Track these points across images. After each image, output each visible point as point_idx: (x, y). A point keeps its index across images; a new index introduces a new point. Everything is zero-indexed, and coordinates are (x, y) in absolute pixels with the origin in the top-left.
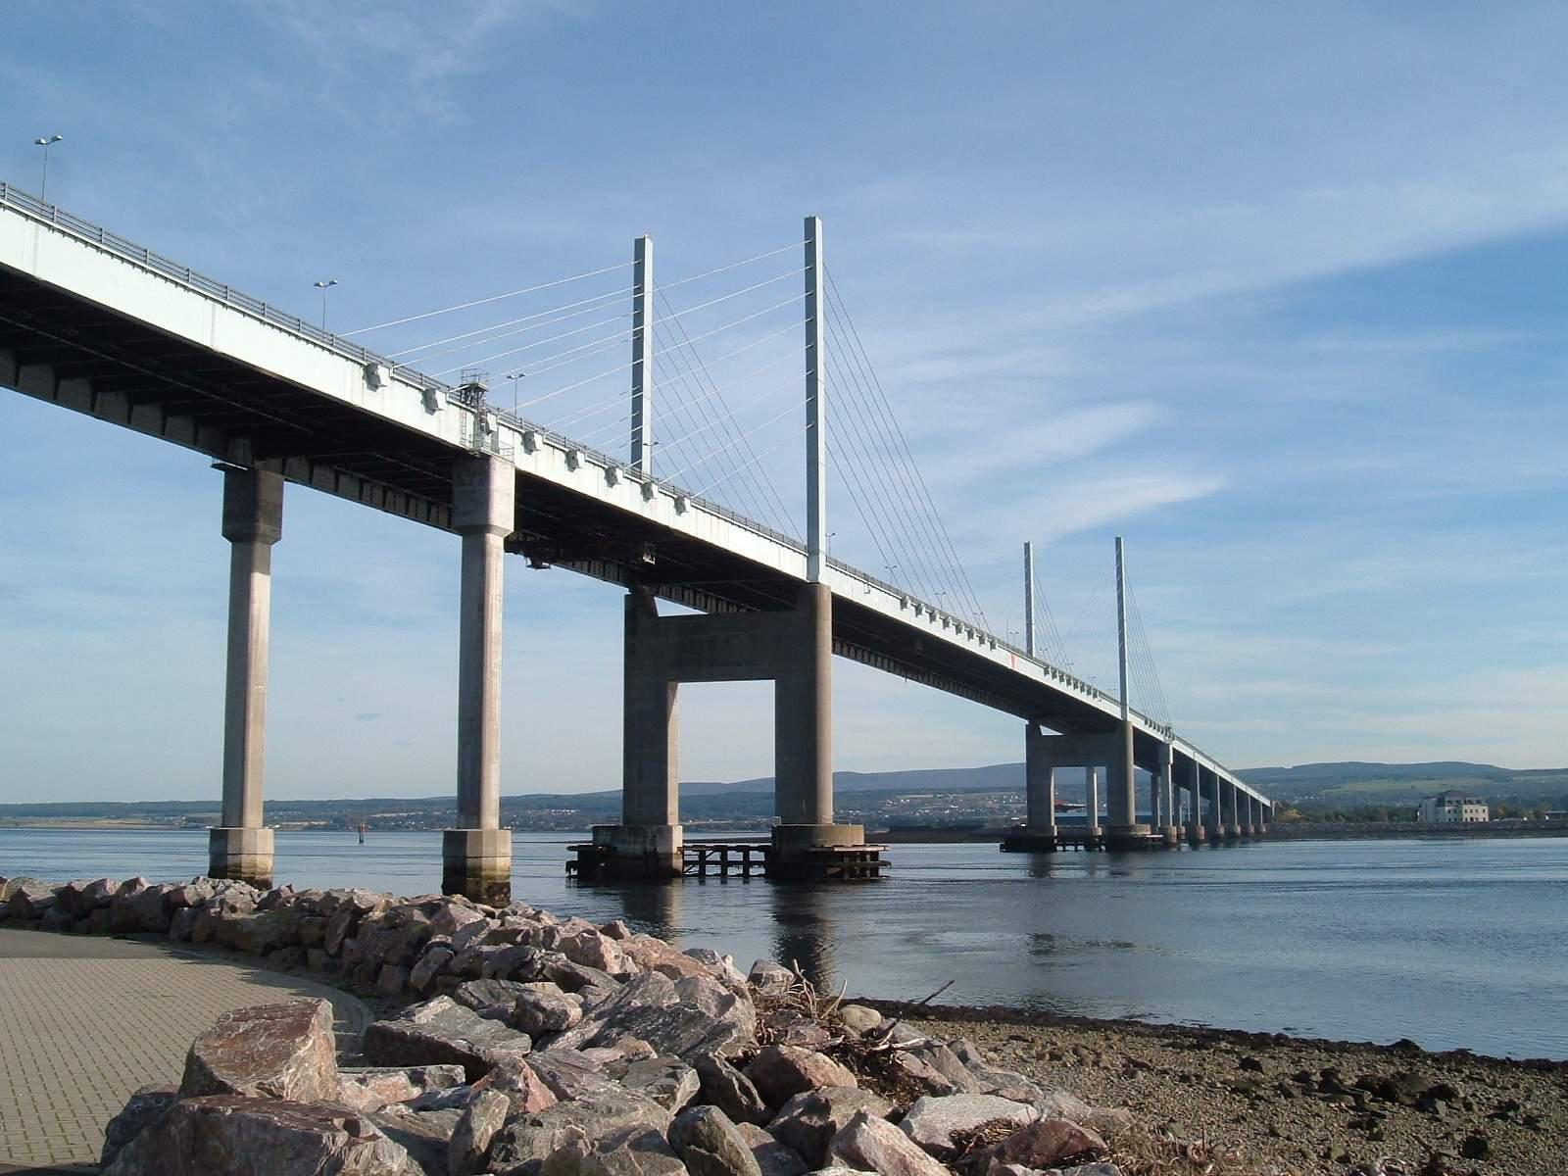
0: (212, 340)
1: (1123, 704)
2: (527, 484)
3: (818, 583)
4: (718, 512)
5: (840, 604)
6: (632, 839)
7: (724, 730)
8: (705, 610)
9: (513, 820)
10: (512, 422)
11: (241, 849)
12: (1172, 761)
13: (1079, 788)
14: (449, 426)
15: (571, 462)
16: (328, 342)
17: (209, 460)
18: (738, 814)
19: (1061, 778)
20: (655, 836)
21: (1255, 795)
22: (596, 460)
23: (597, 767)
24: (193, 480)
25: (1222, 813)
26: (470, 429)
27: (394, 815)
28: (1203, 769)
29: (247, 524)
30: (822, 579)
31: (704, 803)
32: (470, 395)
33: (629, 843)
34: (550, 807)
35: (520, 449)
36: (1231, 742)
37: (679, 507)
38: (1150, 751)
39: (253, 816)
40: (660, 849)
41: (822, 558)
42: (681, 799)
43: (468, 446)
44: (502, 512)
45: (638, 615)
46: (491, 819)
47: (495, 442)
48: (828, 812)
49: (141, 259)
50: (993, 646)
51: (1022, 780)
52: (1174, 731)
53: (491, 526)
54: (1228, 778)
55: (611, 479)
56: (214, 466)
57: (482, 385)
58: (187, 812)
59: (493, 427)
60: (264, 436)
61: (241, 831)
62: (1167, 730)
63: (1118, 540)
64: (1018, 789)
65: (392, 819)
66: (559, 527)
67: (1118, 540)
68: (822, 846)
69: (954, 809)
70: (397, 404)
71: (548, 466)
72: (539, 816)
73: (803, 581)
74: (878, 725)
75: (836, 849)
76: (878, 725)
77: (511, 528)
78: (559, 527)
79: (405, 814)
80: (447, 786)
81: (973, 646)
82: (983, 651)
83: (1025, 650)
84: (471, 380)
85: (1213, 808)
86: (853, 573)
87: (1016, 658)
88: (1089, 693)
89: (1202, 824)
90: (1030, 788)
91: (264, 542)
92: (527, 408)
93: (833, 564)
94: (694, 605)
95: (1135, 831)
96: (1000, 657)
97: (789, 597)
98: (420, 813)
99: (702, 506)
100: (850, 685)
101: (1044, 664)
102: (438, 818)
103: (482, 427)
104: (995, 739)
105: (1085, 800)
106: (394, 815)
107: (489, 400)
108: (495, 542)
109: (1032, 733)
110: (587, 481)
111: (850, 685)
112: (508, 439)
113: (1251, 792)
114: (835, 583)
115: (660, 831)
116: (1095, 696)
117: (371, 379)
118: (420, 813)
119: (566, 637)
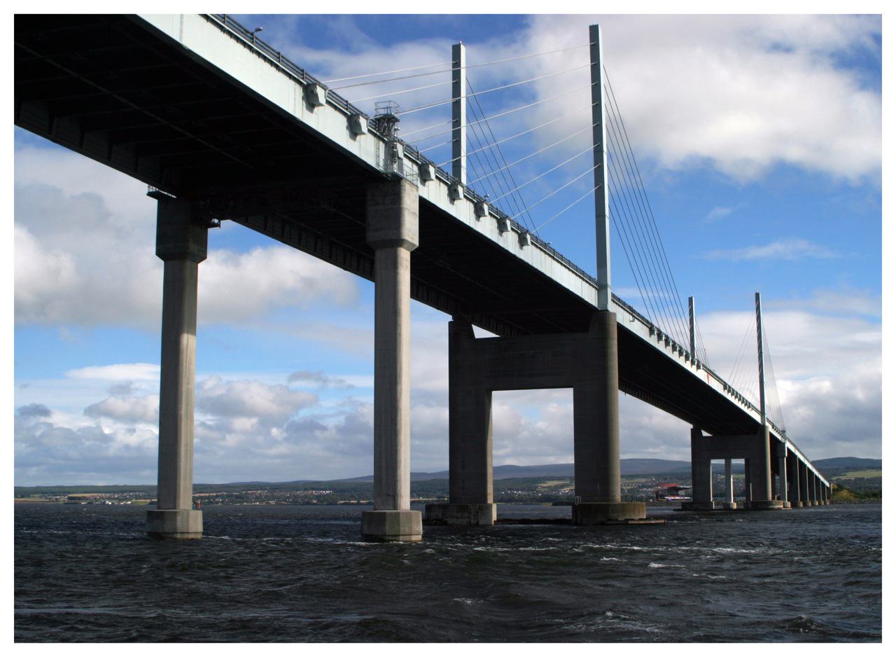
0: (181, 37)
1: (601, 287)
2: (426, 208)
3: (607, 310)
6: (460, 515)
7: (533, 425)
9: (288, 498)
11: (176, 529)
12: (786, 455)
13: (729, 472)
14: (367, 150)
18: (440, 494)
20: (478, 512)
26: (382, 156)
27: (207, 495)
29: (180, 247)
32: (384, 125)
33: (457, 518)
34: (313, 489)
37: (522, 242)
40: (481, 522)
43: (381, 168)
44: (411, 229)
52: (787, 434)
53: (403, 240)
56: (150, 194)
58: (69, 493)
59: (401, 155)
61: (176, 512)
62: (783, 433)
63: (757, 295)
64: (570, 478)
65: (206, 497)
67: (757, 295)
68: (617, 520)
70: (327, 123)
71: (436, 194)
72: (305, 495)
73: (594, 307)
75: (630, 522)
76: (651, 434)
77: (416, 242)
79: (215, 494)
84: (383, 112)
87: (710, 377)
88: (742, 402)
89: (734, 501)
91: (192, 261)
93: (617, 300)
94: (497, 331)
95: (773, 505)
97: (583, 320)
98: (225, 493)
101: (724, 382)
102: (237, 497)
103: (392, 156)
105: (691, 481)
106: (207, 495)
113: (822, 479)
115: (481, 508)
116: (749, 407)
118: (225, 493)
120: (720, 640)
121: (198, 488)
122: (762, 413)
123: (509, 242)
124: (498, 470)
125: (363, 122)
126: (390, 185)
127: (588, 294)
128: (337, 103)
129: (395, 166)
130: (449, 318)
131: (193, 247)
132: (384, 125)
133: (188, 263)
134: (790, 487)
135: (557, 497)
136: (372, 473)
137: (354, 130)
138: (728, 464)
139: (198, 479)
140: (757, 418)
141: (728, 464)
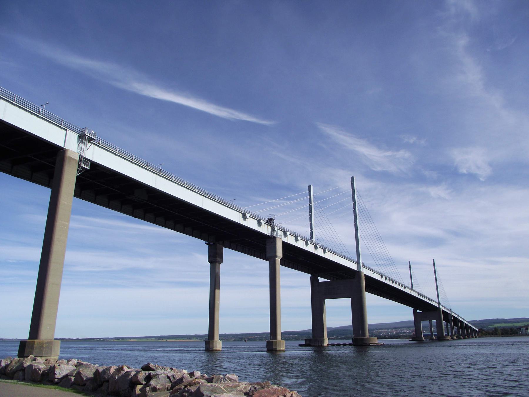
1: (358, 263)
2: (285, 245)
4: (334, 253)
5: (367, 277)
7: (338, 312)
8: (332, 278)
10: (280, 229)
14: (265, 230)
15: (297, 240)
16: (232, 207)
17: (204, 242)
19: (425, 323)
21: (471, 325)
22: (303, 239)
23: (305, 324)
24: (197, 250)
25: (462, 330)
26: (270, 231)
28: (466, 324)
29: (215, 259)
30: (361, 270)
31: (335, 333)
32: (270, 222)
35: (283, 236)
36: (467, 315)
37: (324, 251)
38: (447, 316)
39: (216, 338)
41: (361, 265)
42: (328, 332)
44: (280, 253)
45: (314, 282)
46: (279, 337)
47: (277, 233)
48: (367, 334)
49: (223, 203)
50: (405, 288)
51: (413, 325)
54: (467, 323)
55: (307, 244)
57: (273, 218)
59: (276, 230)
60: (220, 235)
62: (450, 310)
66: (296, 258)
69: (394, 332)
70: (251, 224)
71: (290, 240)
74: (381, 312)
76: (381, 312)
78: (296, 258)
80: (267, 329)
81: (400, 288)
82: (403, 289)
83: (356, 260)
85: (458, 329)
86: (369, 269)
90: (415, 326)
92: (286, 226)
93: (364, 266)
96: (407, 291)
97: (351, 276)
99: (330, 251)
100: (371, 299)
103: (273, 230)
104: (405, 314)
107: (275, 222)
108: (278, 260)
109: (415, 312)
110: (300, 244)
111: (371, 299)
112: (280, 233)
114: (365, 272)
117: (244, 217)
119: (296, 285)
120: (149, 340)
121: (283, 334)
122: (439, 303)
123: (319, 252)
124: (369, 325)
125: (262, 222)
126: (272, 239)
127: (354, 267)
128: (252, 217)
129: (275, 233)
130: (311, 275)
131: (218, 259)
132: (270, 222)
133: (217, 264)
134: (462, 331)
135: (380, 336)
136: (311, 328)
137: (260, 224)
138: (431, 323)
139: (328, 327)
140: (437, 305)
141: (431, 323)
